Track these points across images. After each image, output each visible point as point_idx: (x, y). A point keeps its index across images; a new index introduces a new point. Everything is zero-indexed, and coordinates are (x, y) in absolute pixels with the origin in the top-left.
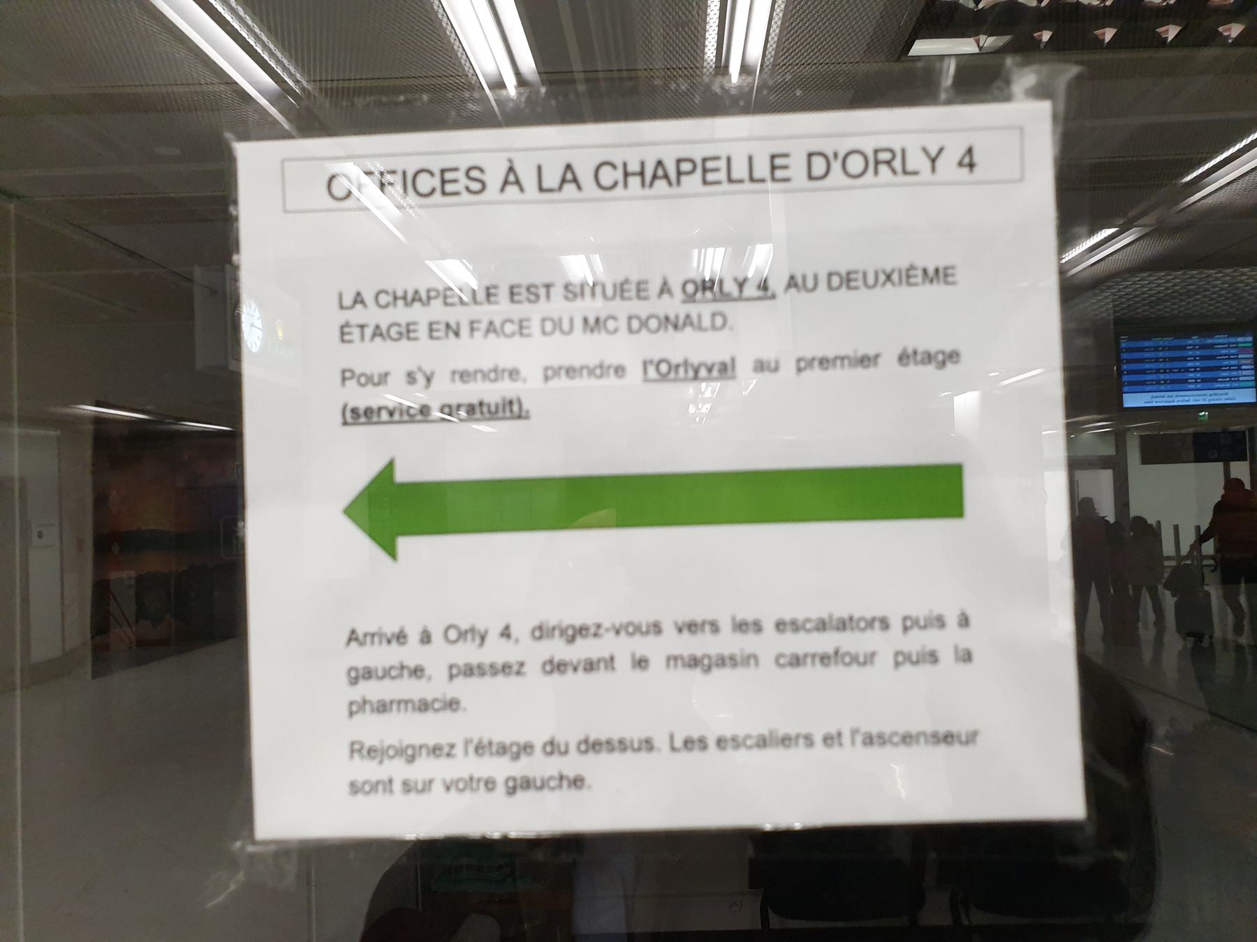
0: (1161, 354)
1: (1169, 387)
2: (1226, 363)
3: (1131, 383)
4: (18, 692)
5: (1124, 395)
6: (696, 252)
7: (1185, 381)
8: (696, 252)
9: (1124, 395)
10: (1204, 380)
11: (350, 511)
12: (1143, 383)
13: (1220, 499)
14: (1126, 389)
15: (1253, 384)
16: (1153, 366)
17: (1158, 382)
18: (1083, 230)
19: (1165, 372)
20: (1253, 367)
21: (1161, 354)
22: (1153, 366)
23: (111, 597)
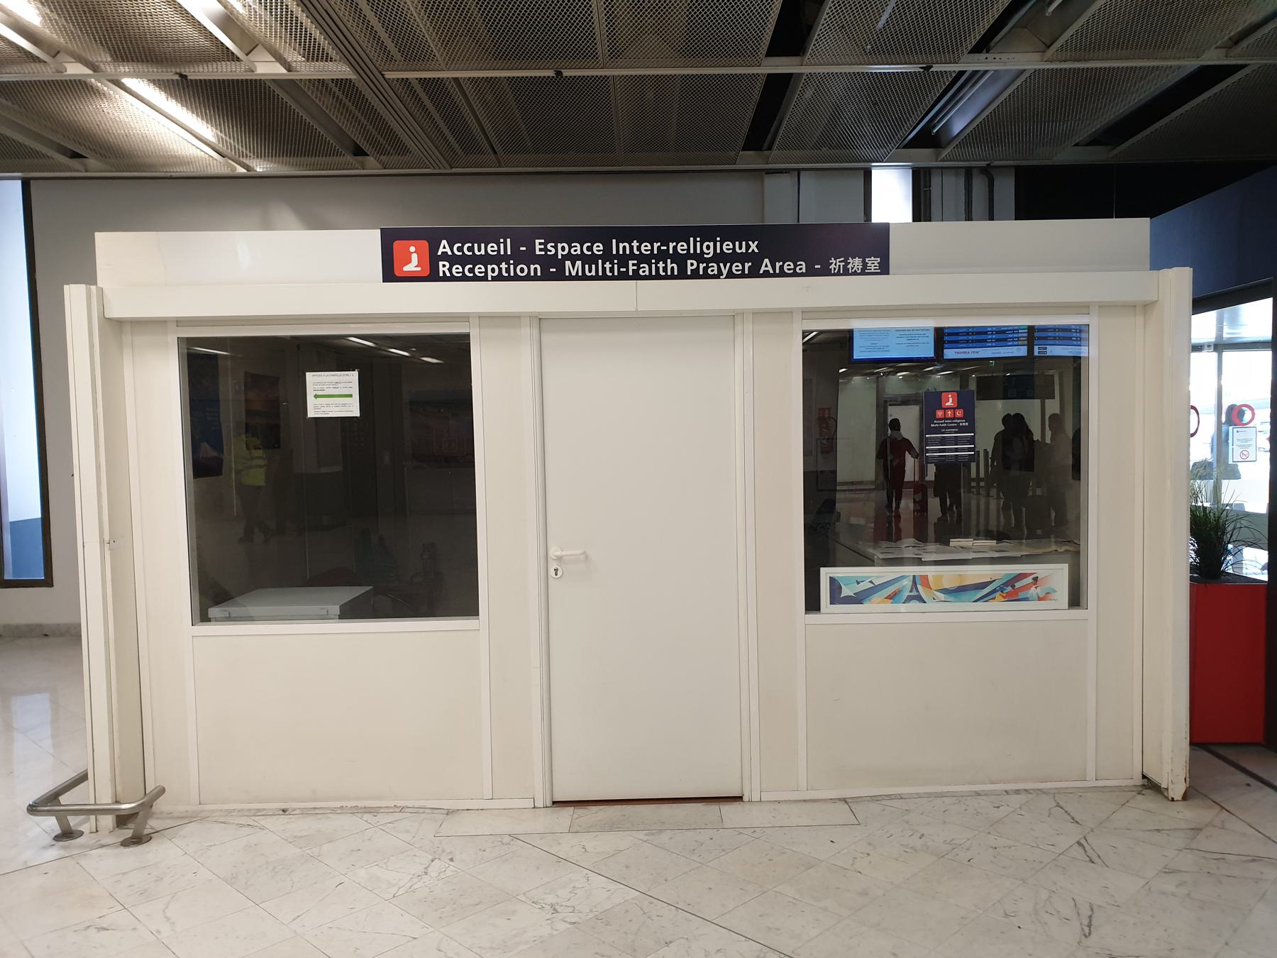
0: (970, 337)
1: (974, 345)
2: (1010, 336)
3: (950, 342)
4: (231, 398)
5: (945, 350)
6: (509, 253)
7: (985, 341)
8: (509, 253)
9: (945, 350)
10: (997, 340)
11: (471, 609)
12: (957, 342)
13: (1002, 428)
14: (946, 346)
15: (1026, 342)
16: (965, 338)
17: (967, 341)
18: (984, 538)
19: (973, 334)
20: (1026, 331)
21: (970, 337)
22: (965, 338)
23: (73, 60)
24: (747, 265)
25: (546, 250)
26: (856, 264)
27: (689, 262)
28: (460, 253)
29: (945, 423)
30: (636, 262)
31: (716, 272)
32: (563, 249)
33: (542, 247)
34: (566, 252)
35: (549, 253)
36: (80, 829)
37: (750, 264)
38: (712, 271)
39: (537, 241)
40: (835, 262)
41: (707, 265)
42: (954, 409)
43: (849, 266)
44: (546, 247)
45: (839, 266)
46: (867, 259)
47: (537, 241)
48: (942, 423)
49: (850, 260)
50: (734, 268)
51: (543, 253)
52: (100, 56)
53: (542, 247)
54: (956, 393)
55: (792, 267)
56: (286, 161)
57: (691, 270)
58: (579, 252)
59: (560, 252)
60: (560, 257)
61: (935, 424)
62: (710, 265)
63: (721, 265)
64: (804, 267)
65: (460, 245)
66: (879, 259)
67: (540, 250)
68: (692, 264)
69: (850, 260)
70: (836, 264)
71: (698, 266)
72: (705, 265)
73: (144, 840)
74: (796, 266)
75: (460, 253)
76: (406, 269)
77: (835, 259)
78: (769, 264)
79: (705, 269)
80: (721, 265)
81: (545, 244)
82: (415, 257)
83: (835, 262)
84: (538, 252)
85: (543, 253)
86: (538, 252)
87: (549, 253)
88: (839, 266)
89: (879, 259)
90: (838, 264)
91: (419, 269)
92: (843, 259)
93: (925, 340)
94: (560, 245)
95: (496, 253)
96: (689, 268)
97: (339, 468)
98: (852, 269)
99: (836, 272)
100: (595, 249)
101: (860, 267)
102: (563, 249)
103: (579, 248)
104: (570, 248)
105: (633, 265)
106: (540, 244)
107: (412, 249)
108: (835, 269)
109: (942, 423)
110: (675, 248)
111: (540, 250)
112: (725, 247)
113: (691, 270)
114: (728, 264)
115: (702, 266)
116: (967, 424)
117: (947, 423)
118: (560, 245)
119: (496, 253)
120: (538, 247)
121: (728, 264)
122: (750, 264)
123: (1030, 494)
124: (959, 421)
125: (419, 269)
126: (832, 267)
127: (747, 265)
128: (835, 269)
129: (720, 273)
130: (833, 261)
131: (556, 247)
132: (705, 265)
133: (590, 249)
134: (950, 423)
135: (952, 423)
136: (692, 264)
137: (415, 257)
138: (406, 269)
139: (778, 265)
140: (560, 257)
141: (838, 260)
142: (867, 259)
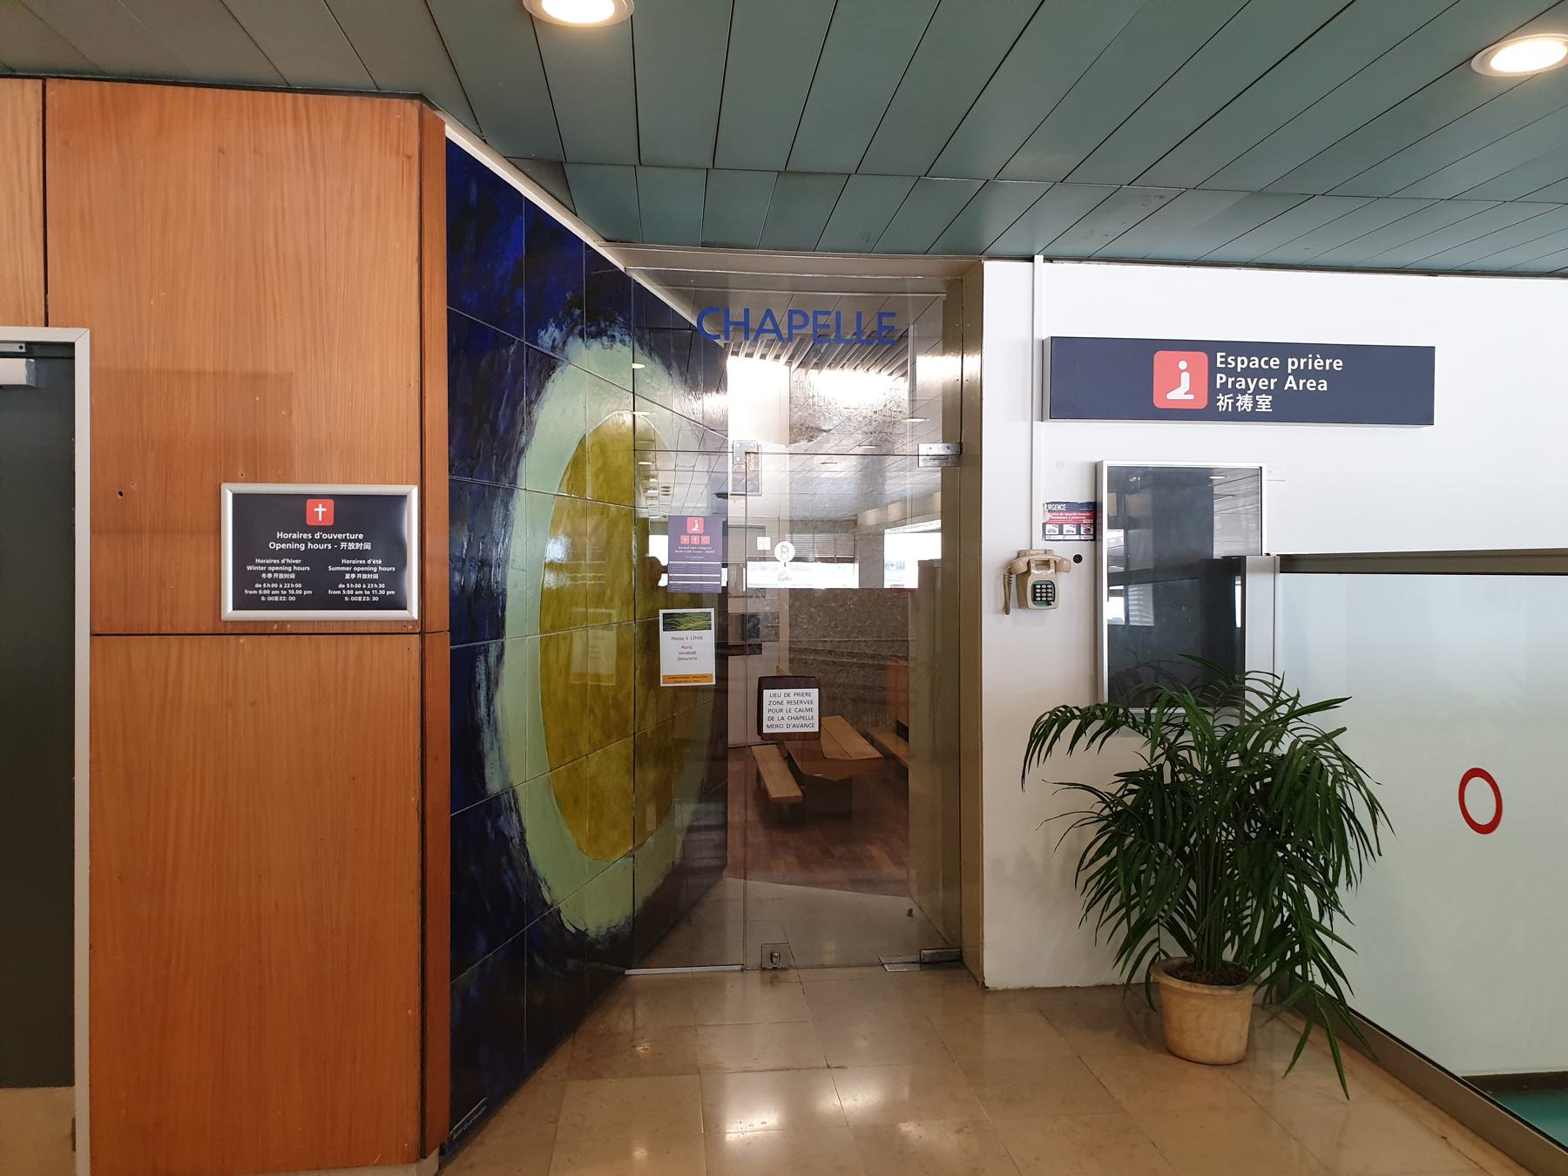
24: (1273, 381)
25: (1226, 363)
26: (1246, 402)
27: (1219, 376)
28: (1267, 367)
29: (689, 550)
30: (1224, 354)
31: (1243, 387)
32: (1243, 362)
33: (1223, 360)
34: (1244, 366)
35: (1229, 366)
37: (1276, 380)
38: (1241, 385)
39: (1219, 354)
40: (1222, 398)
41: (1236, 379)
42: (700, 535)
43: (1239, 404)
44: (1226, 360)
45: (1228, 403)
46: (1257, 397)
47: (1219, 354)
49: (1240, 397)
50: (1260, 384)
51: (1224, 366)
52: (1299, 761)
53: (1223, 360)
55: (1314, 384)
57: (1221, 384)
58: (1257, 366)
59: (1239, 366)
60: (1239, 370)
62: (1238, 379)
63: (1249, 380)
64: (1325, 385)
65: (1267, 359)
66: (1270, 397)
67: (1221, 363)
68: (1221, 378)
69: (1240, 397)
70: (1223, 401)
71: (1227, 380)
72: (1233, 379)
74: (1318, 384)
75: (1267, 367)
77: (1223, 396)
78: (1293, 382)
79: (1234, 383)
80: (1249, 380)
81: (1226, 357)
83: (1222, 398)
84: (1219, 365)
85: (1224, 366)
86: (1219, 365)
87: (1229, 366)
88: (1228, 403)
89: (1270, 397)
90: (1226, 401)
92: (1231, 395)
94: (1239, 359)
95: (1321, 368)
96: (1219, 382)
98: (1242, 407)
99: (1224, 409)
100: (1272, 363)
101: (1250, 405)
102: (1243, 362)
103: (1257, 362)
104: (1249, 361)
105: (1221, 357)
106: (1221, 357)
107: (1183, 365)
108: (1223, 407)
110: (1331, 364)
111: (1221, 363)
112: (1316, 364)
113: (1221, 384)
114: (1255, 380)
115: (1230, 380)
117: (692, 550)
118: (1239, 359)
119: (1321, 368)
120: (1219, 360)
121: (1255, 380)
122: (1276, 380)
126: (1220, 404)
127: (1273, 381)
128: (1223, 407)
129: (1248, 387)
130: (1221, 397)
131: (1236, 360)
132: (1233, 379)
133: (1267, 363)
134: (695, 550)
135: (698, 550)
136: (1221, 378)
139: (1301, 382)
140: (1239, 370)
141: (1226, 397)
142: (1257, 397)
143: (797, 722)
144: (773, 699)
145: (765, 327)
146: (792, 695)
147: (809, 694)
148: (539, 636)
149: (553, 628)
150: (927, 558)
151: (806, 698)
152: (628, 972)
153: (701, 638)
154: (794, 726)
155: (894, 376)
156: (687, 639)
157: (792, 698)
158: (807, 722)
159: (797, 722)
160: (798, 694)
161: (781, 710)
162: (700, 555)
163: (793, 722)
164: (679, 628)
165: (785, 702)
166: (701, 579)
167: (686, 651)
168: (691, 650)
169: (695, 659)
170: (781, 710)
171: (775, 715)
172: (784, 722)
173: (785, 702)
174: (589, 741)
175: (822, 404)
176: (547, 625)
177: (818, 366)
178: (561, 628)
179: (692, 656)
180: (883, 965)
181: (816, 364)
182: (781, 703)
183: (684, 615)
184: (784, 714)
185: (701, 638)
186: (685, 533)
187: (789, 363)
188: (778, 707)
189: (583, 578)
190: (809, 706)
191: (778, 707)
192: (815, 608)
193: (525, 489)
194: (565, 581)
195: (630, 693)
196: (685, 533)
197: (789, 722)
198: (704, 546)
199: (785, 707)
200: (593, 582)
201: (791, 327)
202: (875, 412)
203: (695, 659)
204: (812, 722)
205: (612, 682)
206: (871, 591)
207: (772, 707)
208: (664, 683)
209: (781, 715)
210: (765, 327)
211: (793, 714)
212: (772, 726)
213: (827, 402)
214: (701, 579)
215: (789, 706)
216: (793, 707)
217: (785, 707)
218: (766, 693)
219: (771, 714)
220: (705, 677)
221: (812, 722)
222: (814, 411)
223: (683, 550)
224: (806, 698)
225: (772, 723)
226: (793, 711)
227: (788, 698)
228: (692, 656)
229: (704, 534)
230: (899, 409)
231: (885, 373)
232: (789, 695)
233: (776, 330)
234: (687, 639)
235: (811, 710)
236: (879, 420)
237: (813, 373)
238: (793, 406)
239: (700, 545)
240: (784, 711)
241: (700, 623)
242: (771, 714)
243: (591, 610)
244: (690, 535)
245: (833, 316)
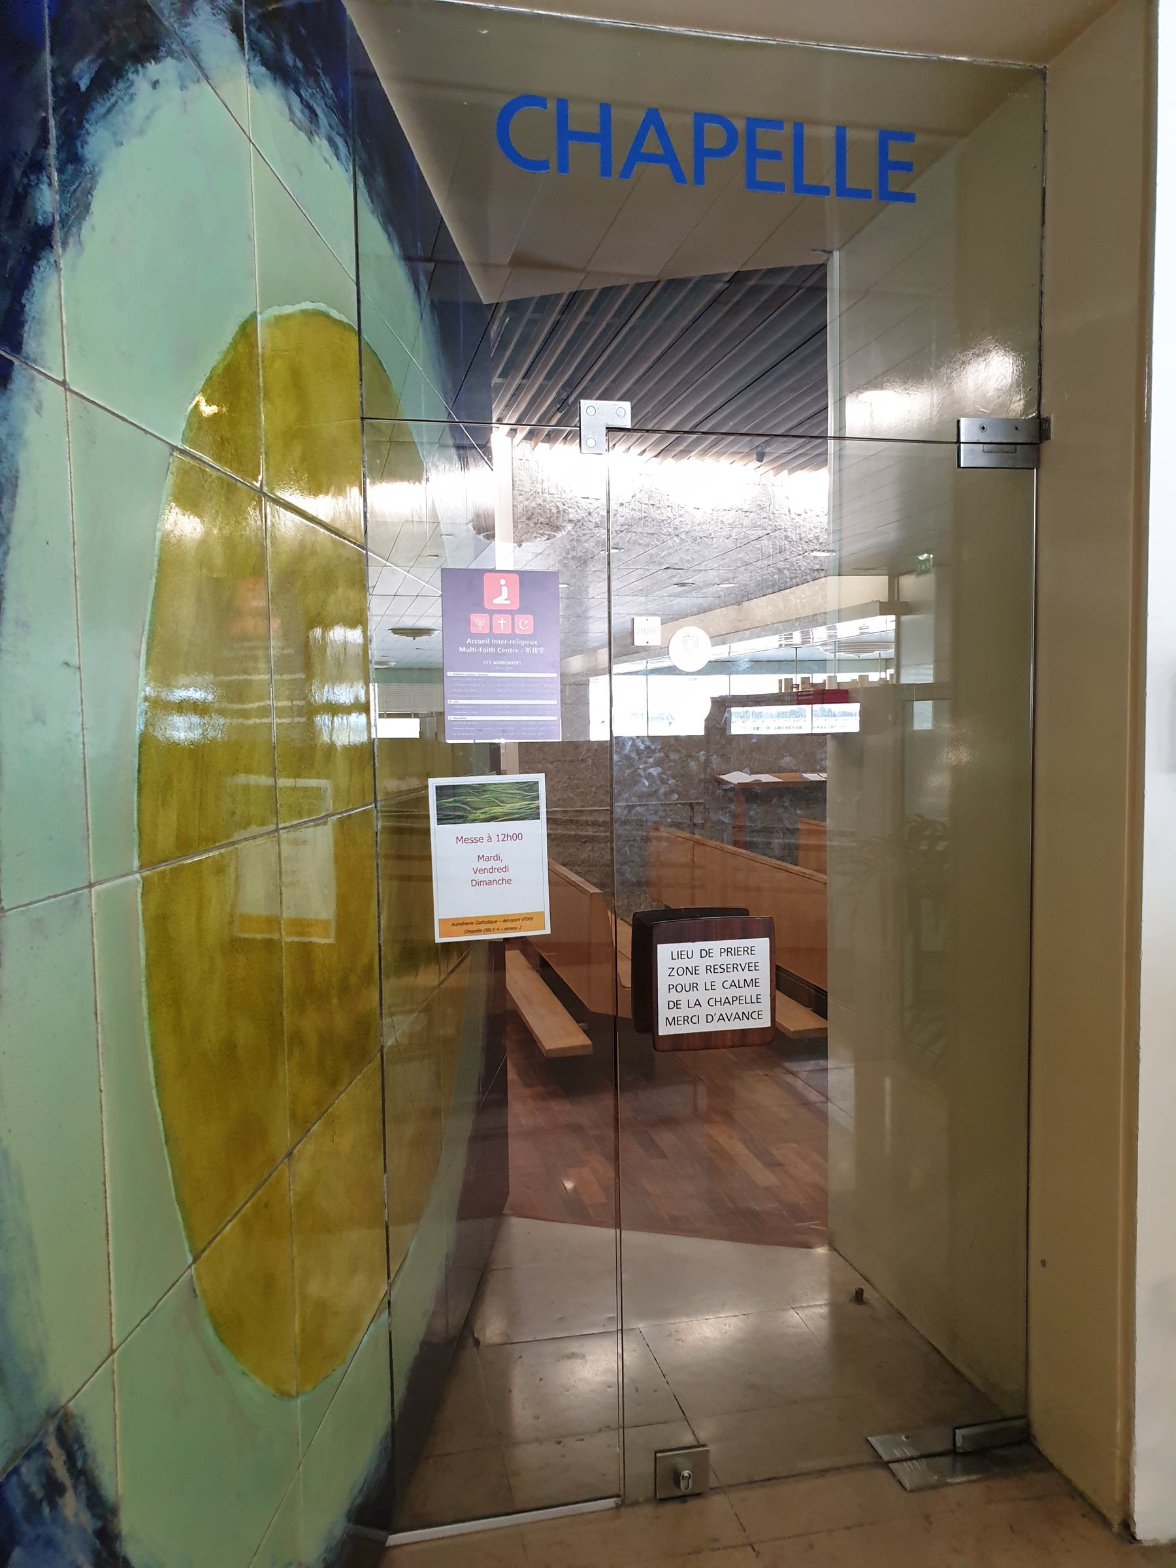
29: (490, 645)
36: (908, 191)
42: (512, 613)
48: (484, 646)
54: (516, 576)
56: (810, 832)
61: (468, 646)
73: (677, 672)
76: (496, 601)
82: (505, 590)
91: (508, 602)
93: (602, 596)
97: (331, 941)
109: (484, 646)
116: (542, 650)
117: (496, 646)
123: (932, 556)
124: (523, 643)
125: (508, 602)
135: (511, 646)
137: (505, 590)
138: (496, 601)
143: (727, 1009)
144: (677, 963)
145: (645, 149)
146: (716, 953)
147: (750, 951)
148: (138, 876)
149: (185, 846)
150: (717, 695)
151: (744, 959)
152: (394, 1539)
153: (518, 837)
154: (721, 1018)
155: (647, 455)
156: (490, 839)
157: (717, 959)
158: (748, 1008)
159: (727, 1009)
160: (728, 951)
161: (694, 986)
162: (513, 657)
163: (718, 1010)
164: (471, 817)
165: (702, 970)
166: (515, 710)
167: (488, 865)
168: (497, 864)
169: (508, 881)
170: (694, 986)
171: (683, 997)
172: (702, 1011)
173: (702, 970)
174: (293, 1116)
175: (553, 491)
176: (165, 839)
177: (550, 438)
178: (209, 841)
179: (497, 876)
180: (886, 1465)
181: (548, 435)
182: (694, 971)
183: (481, 789)
184: (703, 996)
185: (518, 837)
186: (479, 607)
187: (513, 432)
188: (688, 979)
189: (265, 712)
190: (749, 975)
191: (688, 979)
192: (552, 763)
193: (63, 383)
194: (217, 727)
195: (371, 961)
196: (479, 607)
197: (712, 1011)
198: (523, 637)
199: (703, 978)
200: (287, 720)
201: (701, 152)
202: (622, 504)
203: (508, 881)
204: (756, 1007)
205: (327, 936)
206: (575, 745)
207: (676, 980)
208: (441, 937)
209: (693, 996)
210: (645, 149)
211: (720, 993)
212: (676, 1021)
213: (560, 489)
214: (515, 710)
215: (711, 977)
216: (719, 978)
217: (703, 978)
218: (665, 952)
219: (674, 996)
220: (529, 918)
221: (756, 1007)
222: (544, 501)
223: (478, 646)
224: (744, 959)
225: (675, 1013)
226: (718, 985)
227: (708, 961)
228: (497, 876)
229: (522, 610)
230: (651, 502)
231: (636, 450)
232: (709, 953)
233: (669, 157)
234: (490, 839)
235: (754, 982)
236: (627, 515)
237: (543, 447)
238: (516, 493)
239: (513, 636)
240: (701, 987)
241: (517, 805)
242: (674, 996)
243: (284, 782)
244: (492, 612)
245: (788, 130)
